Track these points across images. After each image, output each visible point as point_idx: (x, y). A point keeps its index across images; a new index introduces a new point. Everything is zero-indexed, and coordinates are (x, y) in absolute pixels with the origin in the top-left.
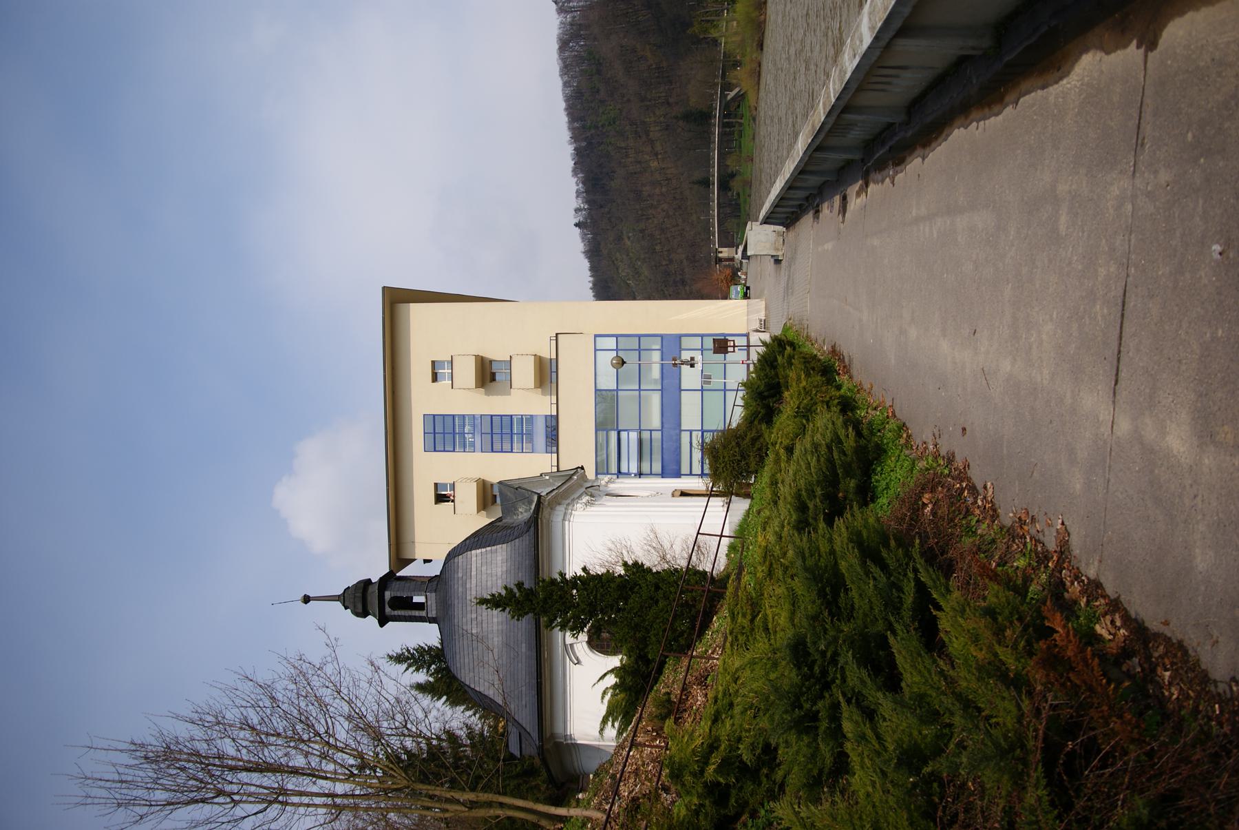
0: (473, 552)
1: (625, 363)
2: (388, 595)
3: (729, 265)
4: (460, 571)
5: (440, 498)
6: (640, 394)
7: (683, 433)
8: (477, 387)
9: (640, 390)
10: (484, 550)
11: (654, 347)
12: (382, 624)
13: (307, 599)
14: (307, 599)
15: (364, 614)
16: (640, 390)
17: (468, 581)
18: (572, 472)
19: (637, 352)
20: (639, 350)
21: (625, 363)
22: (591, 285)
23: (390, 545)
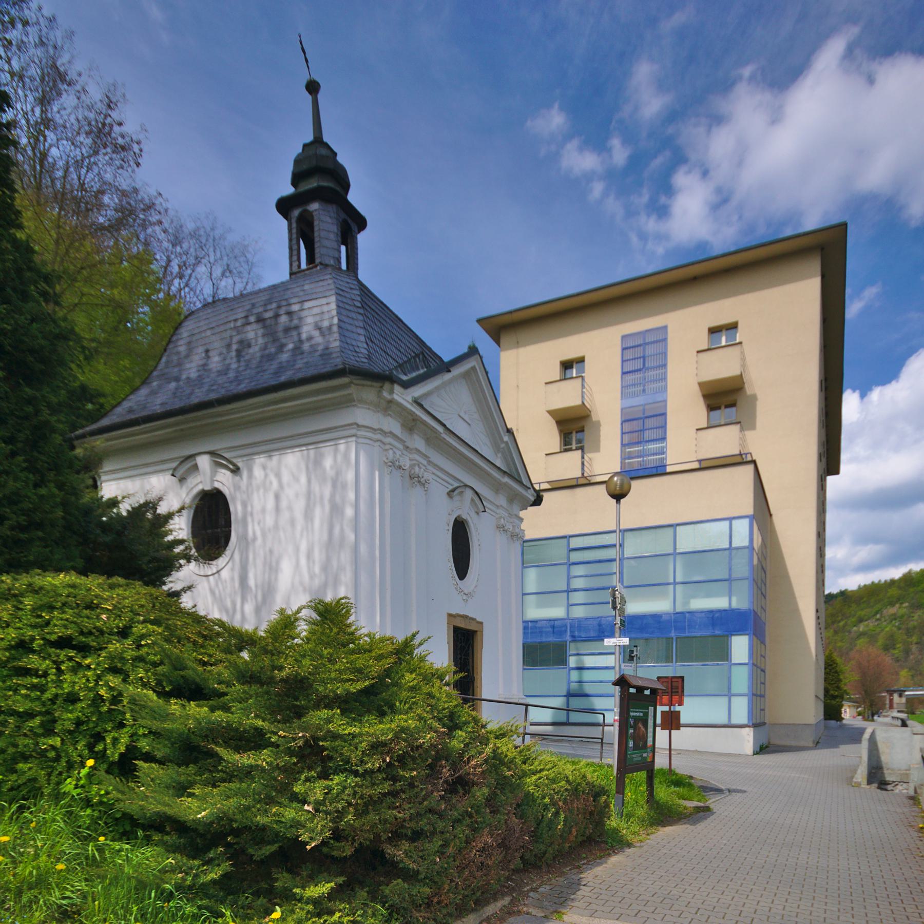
0: (333, 299)
1: (618, 501)
2: (314, 206)
3: (163, 722)
4: (312, 286)
5: (567, 365)
6: (669, 584)
7: (734, 668)
8: (701, 385)
9: (675, 583)
10: (334, 313)
11: (632, 562)
12: (284, 206)
13: (313, 88)
14: (313, 88)
15: (296, 179)
16: (675, 583)
17: (688, 540)
18: (525, 482)
19: (727, 577)
20: (729, 580)
21: (618, 501)
22: (876, 581)
23: (511, 312)
